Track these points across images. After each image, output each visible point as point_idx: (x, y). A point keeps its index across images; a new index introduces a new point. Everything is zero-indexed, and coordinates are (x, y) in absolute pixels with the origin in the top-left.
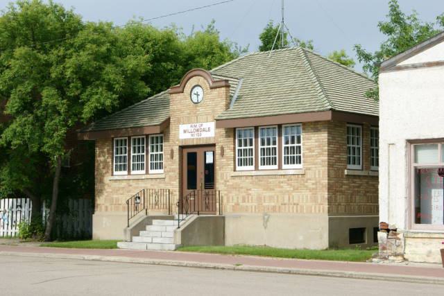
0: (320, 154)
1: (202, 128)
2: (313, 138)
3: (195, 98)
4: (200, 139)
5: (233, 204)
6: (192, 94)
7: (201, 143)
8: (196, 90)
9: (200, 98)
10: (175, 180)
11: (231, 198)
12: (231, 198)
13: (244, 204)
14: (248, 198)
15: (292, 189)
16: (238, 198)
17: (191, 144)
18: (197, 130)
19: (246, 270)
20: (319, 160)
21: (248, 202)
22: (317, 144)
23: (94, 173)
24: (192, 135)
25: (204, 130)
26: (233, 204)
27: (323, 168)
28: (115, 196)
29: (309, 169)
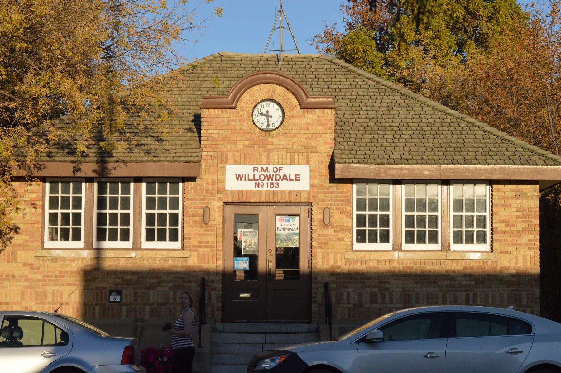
0: (525, 231)
1: (282, 174)
2: (514, 209)
3: (262, 122)
4: (275, 193)
5: (351, 306)
6: (256, 112)
7: (279, 199)
8: (273, 109)
9: (275, 122)
10: (536, 218)
11: (345, 296)
12: (345, 296)
13: (375, 305)
14: (383, 296)
15: (473, 282)
16: (360, 295)
17: (252, 200)
18: (270, 177)
19: (59, 162)
20: (524, 239)
21: (383, 302)
22: (520, 214)
23: (542, 291)
24: (257, 185)
25: (285, 178)
26: (351, 306)
27: (532, 252)
28: (50, 288)
29: (507, 252)
